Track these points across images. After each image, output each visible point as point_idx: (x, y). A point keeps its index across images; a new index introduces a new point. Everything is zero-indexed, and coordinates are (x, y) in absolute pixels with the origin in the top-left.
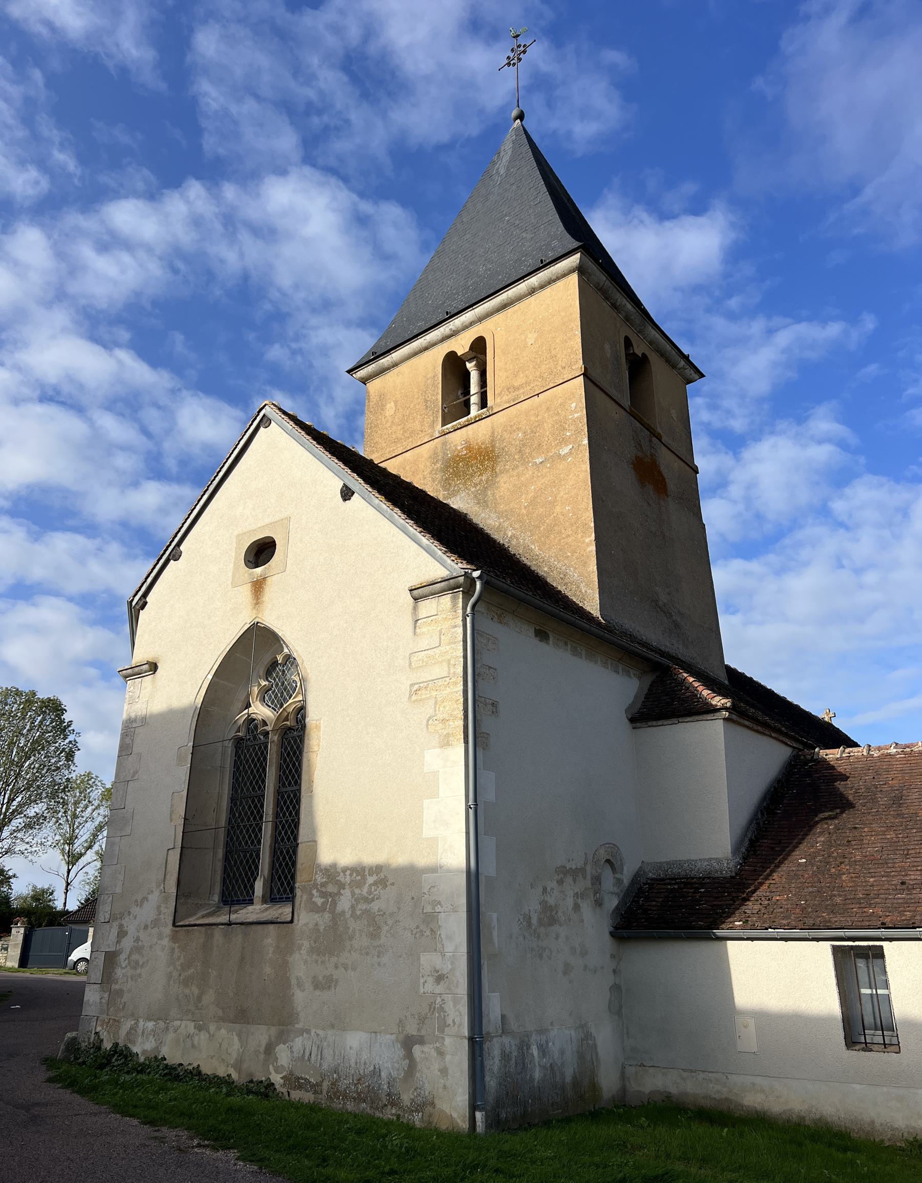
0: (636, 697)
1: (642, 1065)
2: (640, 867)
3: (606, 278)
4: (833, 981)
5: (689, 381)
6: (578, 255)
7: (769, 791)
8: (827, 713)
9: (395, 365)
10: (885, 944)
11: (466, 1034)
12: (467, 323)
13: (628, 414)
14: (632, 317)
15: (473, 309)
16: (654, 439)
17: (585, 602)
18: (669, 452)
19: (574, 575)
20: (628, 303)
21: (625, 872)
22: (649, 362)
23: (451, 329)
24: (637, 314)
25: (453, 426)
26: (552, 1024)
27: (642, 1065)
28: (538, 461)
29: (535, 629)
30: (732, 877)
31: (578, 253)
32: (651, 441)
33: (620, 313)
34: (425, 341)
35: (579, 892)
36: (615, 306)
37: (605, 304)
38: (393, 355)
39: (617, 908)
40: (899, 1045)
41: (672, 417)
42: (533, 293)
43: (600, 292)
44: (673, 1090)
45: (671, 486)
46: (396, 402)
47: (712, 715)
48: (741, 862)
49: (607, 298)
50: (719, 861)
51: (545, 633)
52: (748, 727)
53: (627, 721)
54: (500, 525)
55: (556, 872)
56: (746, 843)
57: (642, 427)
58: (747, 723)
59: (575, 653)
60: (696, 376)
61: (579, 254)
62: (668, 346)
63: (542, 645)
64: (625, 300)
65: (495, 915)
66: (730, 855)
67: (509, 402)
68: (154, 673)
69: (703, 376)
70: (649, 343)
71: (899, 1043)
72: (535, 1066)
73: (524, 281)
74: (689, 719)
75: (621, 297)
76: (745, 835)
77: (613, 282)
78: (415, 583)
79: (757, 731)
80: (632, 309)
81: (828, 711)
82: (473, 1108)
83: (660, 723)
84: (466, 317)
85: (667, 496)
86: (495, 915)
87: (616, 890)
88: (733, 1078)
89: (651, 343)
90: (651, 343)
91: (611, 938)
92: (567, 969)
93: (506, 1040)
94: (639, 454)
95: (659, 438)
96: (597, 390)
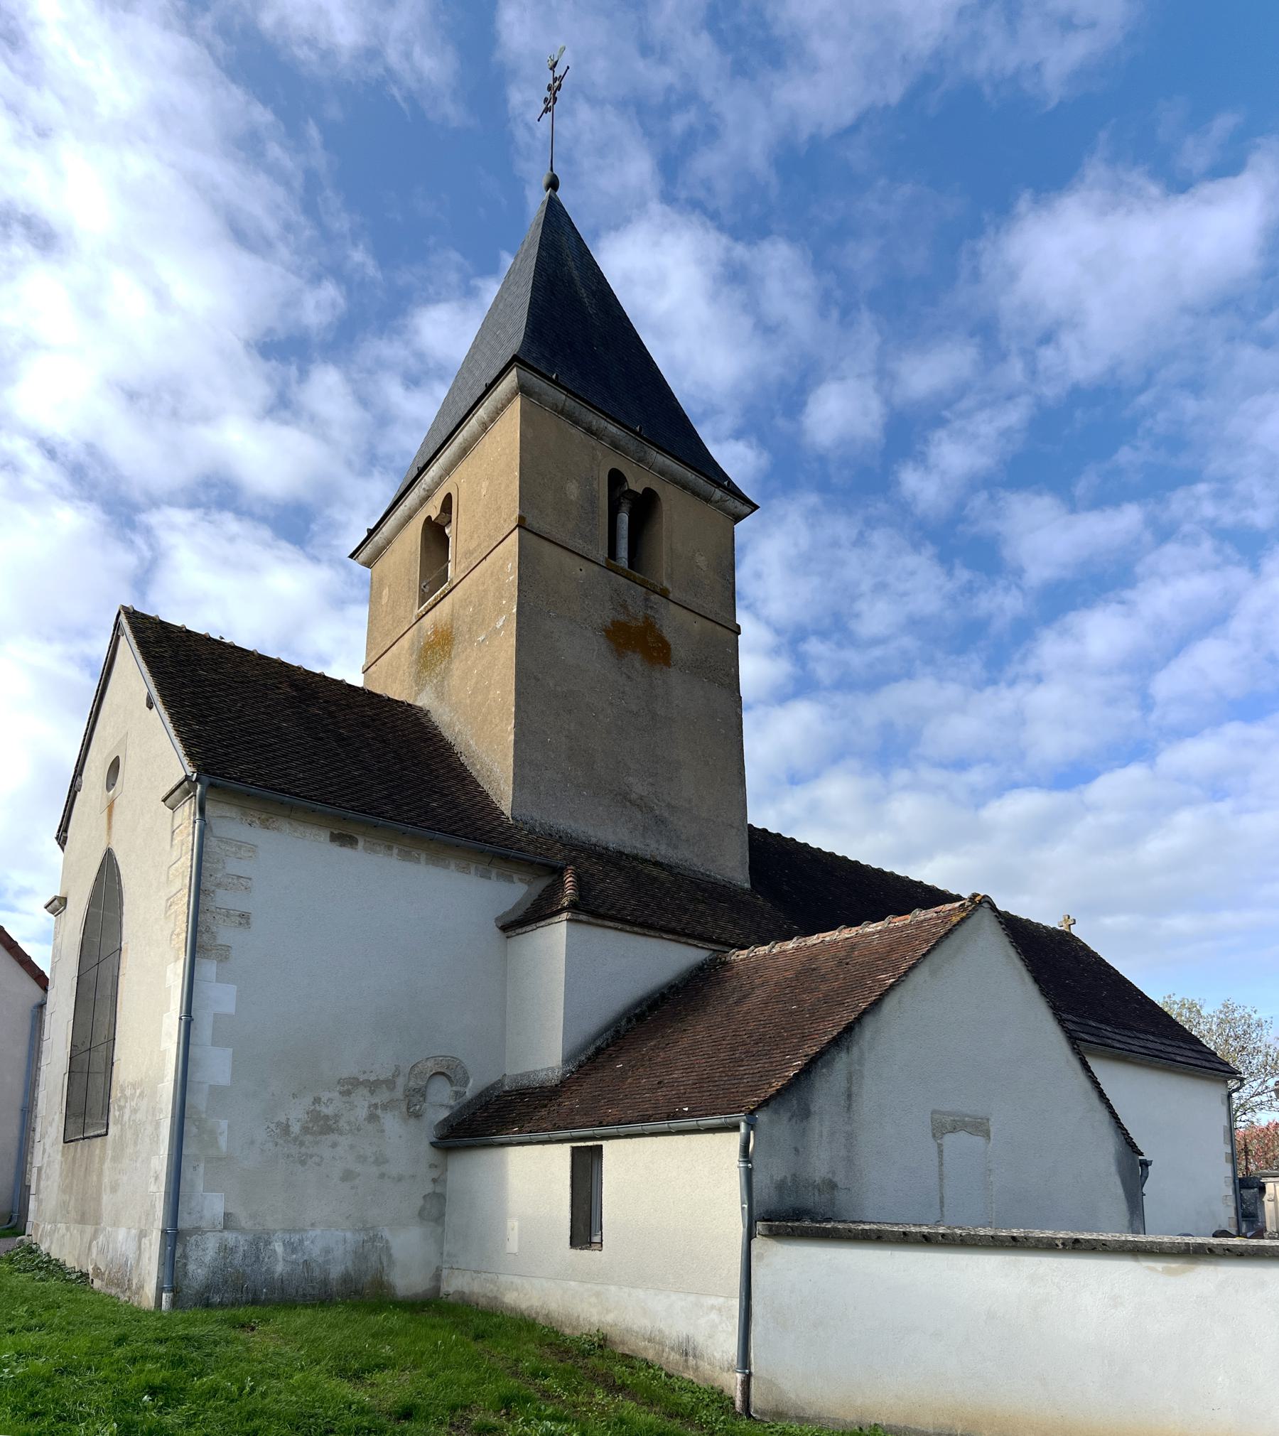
0: (518, 904)
1: (452, 1268)
2: (499, 1080)
3: (566, 395)
4: (568, 1182)
5: (738, 518)
6: (514, 372)
7: (649, 997)
8: (1065, 920)
9: (389, 542)
10: (603, 1143)
11: (161, 1228)
12: (436, 479)
13: (606, 570)
14: (621, 443)
15: (438, 460)
16: (655, 597)
17: (502, 802)
18: (685, 611)
19: (497, 769)
20: (609, 425)
21: (470, 1085)
22: (660, 500)
23: (424, 489)
24: (629, 437)
25: (425, 608)
26: (313, 1225)
27: (452, 1268)
28: (480, 639)
29: (332, 833)
30: (556, 1085)
31: (514, 368)
32: (646, 600)
33: (602, 439)
34: (406, 508)
35: (380, 1104)
36: (590, 431)
37: (573, 431)
38: (384, 529)
39: (445, 1120)
40: (601, 1243)
41: (698, 567)
42: (486, 429)
43: (562, 415)
44: (466, 1290)
45: (680, 651)
46: (390, 586)
47: (558, 917)
48: (573, 1070)
49: (576, 422)
50: (552, 1069)
51: (351, 837)
52: (616, 929)
53: (497, 930)
54: (451, 720)
55: (338, 1083)
56: (592, 1049)
57: (629, 582)
58: (611, 924)
59: (405, 856)
60: (747, 509)
61: (515, 369)
62: (690, 474)
63: (346, 852)
64: (603, 421)
65: (224, 1124)
66: (560, 1063)
67: (463, 571)
68: (65, 908)
69: (756, 507)
70: (659, 473)
71: (602, 1240)
72: (277, 1260)
73: (474, 415)
74: (543, 923)
75: (597, 417)
76: (594, 1039)
77: (577, 400)
78: (164, 794)
79: (644, 935)
80: (619, 432)
81: (1067, 917)
82: (160, 1290)
83: (524, 929)
84: (433, 471)
85: (668, 664)
86: (224, 1124)
87: (452, 1103)
88: (502, 1278)
89: (662, 473)
90: (662, 473)
91: (433, 1149)
92: (348, 1176)
93: (230, 1237)
94: (622, 618)
95: (664, 594)
96: (546, 543)
